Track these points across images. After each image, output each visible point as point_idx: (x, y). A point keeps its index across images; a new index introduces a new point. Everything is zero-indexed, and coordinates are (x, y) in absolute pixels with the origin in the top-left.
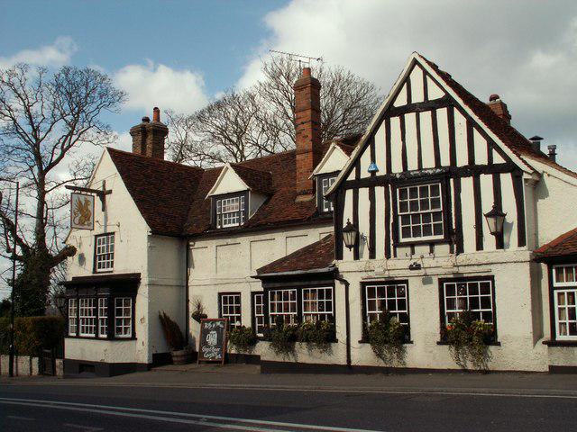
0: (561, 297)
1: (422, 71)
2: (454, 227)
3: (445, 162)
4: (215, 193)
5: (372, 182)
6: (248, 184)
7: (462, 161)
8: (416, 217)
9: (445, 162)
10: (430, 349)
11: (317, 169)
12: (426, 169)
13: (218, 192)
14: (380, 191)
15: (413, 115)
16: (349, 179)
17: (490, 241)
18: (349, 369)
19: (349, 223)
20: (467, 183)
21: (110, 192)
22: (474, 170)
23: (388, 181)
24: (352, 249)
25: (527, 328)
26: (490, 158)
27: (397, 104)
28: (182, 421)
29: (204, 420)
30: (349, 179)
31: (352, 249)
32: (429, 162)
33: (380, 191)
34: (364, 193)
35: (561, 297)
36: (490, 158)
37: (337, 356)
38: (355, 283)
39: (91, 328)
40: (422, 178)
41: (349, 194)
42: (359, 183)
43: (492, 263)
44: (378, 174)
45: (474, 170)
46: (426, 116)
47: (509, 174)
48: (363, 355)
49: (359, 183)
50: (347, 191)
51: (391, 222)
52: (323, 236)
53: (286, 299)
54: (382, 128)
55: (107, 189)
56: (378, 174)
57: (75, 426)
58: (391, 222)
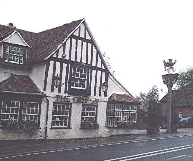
0: (90, 114)
1: (84, 27)
3: (89, 63)
4: (7, 41)
7: (94, 65)
8: (81, 80)
9: (89, 63)
10: (77, 131)
11: (6, 39)
12: (83, 63)
13: (9, 41)
14: (65, 65)
17: (103, 93)
18: (45, 140)
19: (57, 76)
20: (94, 72)
22: (96, 68)
23: (68, 62)
24: (58, 87)
26: (101, 66)
28: (129, 159)
30: (53, 56)
31: (58, 87)
32: (84, 61)
33: (65, 65)
36: (101, 66)
37: (40, 136)
38: (51, 101)
39: (116, 115)
40: (80, 65)
43: (50, 97)
44: (65, 58)
45: (96, 68)
48: (51, 134)
51: (69, 79)
53: (13, 106)
54: (69, 40)
56: (65, 58)
57: (173, 158)
58: (69, 79)
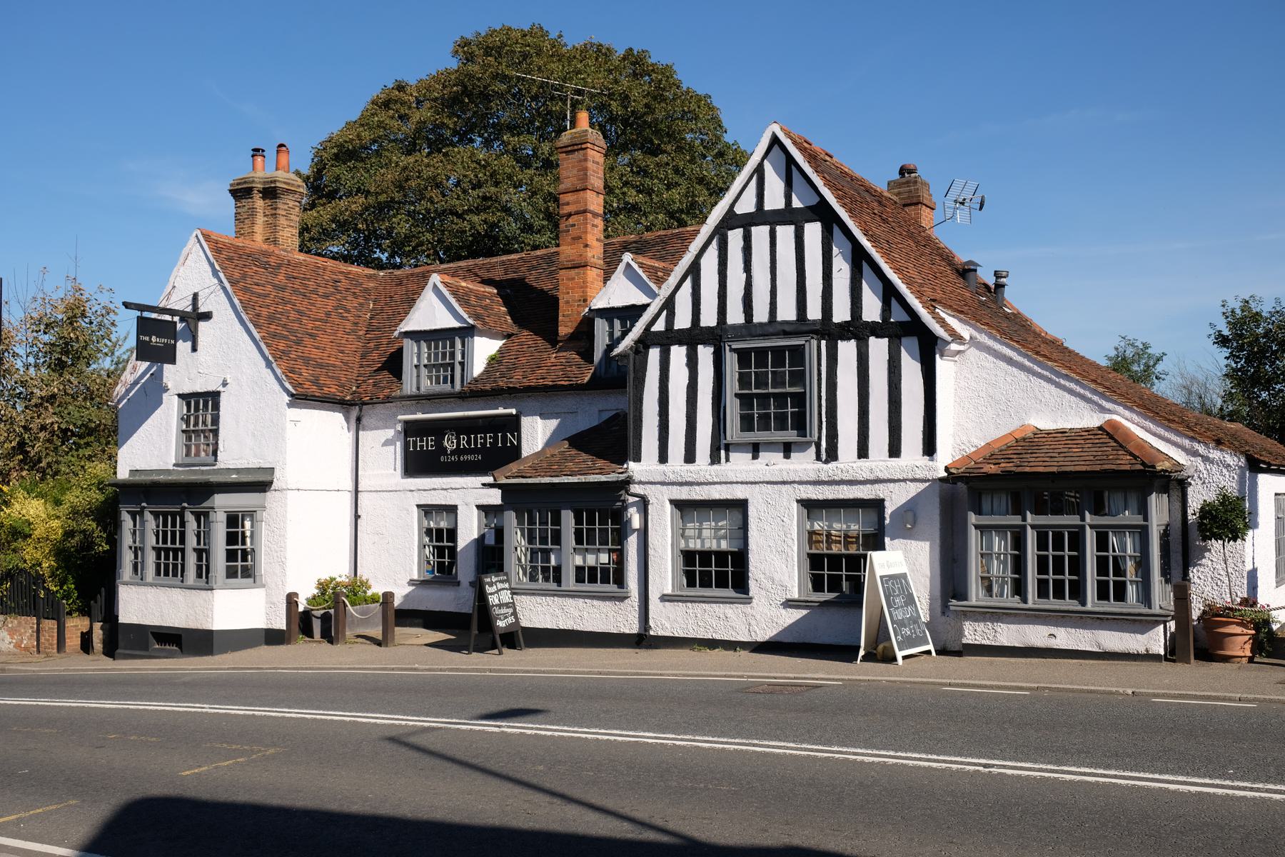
2: (210, 403)
3: (814, 312)
5: (693, 337)
6: (654, 332)
7: (841, 313)
9: (814, 312)
15: (765, 229)
16: (654, 329)
20: (847, 350)
21: (207, 316)
23: (717, 337)
25: (606, 606)
27: (740, 209)
29: (1168, 638)
30: (654, 329)
32: (787, 312)
34: (678, 354)
35: (534, 555)
41: (654, 354)
42: (668, 339)
46: (786, 233)
47: (886, 340)
49: (668, 339)
50: (651, 350)
52: (606, 416)
55: (202, 309)
